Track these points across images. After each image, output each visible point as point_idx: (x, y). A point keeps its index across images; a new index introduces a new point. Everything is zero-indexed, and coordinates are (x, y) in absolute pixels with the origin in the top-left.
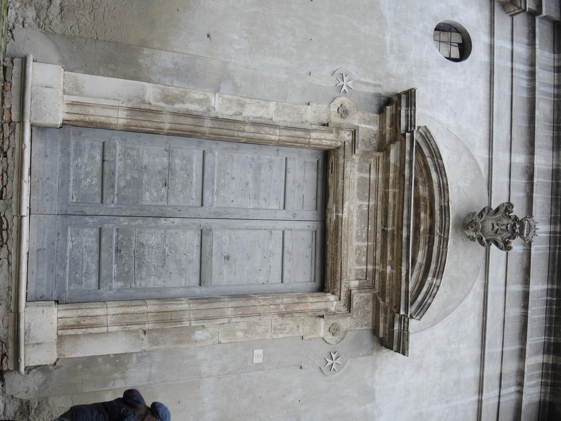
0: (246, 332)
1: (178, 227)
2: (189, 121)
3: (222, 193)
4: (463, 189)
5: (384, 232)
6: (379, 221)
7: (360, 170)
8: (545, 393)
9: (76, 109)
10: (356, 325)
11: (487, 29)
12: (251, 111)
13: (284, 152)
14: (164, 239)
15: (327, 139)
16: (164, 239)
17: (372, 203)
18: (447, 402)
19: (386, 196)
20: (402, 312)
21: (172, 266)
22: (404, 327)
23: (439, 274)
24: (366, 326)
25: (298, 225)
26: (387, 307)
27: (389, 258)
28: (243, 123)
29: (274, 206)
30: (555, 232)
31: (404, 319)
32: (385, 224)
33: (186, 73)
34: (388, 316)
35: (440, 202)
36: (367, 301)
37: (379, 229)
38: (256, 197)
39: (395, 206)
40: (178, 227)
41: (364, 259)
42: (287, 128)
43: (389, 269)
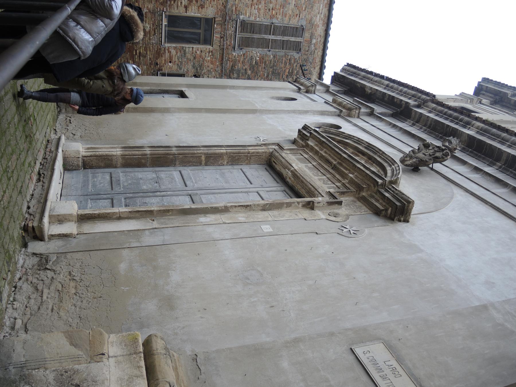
5: (334, 168)
20: (380, 181)
22: (393, 191)
26: (371, 194)
31: (389, 188)
34: (376, 196)
35: (363, 146)
39: (329, 155)
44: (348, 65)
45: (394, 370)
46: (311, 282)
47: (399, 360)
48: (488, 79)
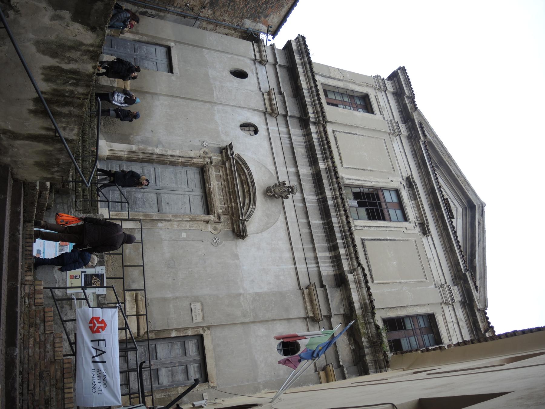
0: (178, 226)
1: (148, 192)
2: (148, 155)
3: (163, 182)
4: (261, 178)
5: (229, 192)
6: (227, 189)
7: (216, 171)
8: (336, 270)
9: (111, 152)
10: (224, 227)
11: (265, 124)
12: (170, 153)
13: (185, 168)
14: (143, 196)
15: (201, 161)
16: (143, 196)
17: (223, 183)
18: (277, 266)
19: (227, 179)
20: (241, 218)
21: (147, 205)
23: (255, 204)
24: (229, 228)
25: (195, 194)
27: (233, 200)
28: (167, 155)
29: (184, 187)
30: (319, 199)
32: (229, 189)
33: (146, 142)
36: (228, 219)
37: (227, 192)
38: (176, 183)
40: (148, 192)
41: (223, 203)
42: (183, 157)
43: (233, 204)
44: (304, 38)
45: (199, 313)
46: (190, 270)
47: (202, 310)
48: (405, 70)
